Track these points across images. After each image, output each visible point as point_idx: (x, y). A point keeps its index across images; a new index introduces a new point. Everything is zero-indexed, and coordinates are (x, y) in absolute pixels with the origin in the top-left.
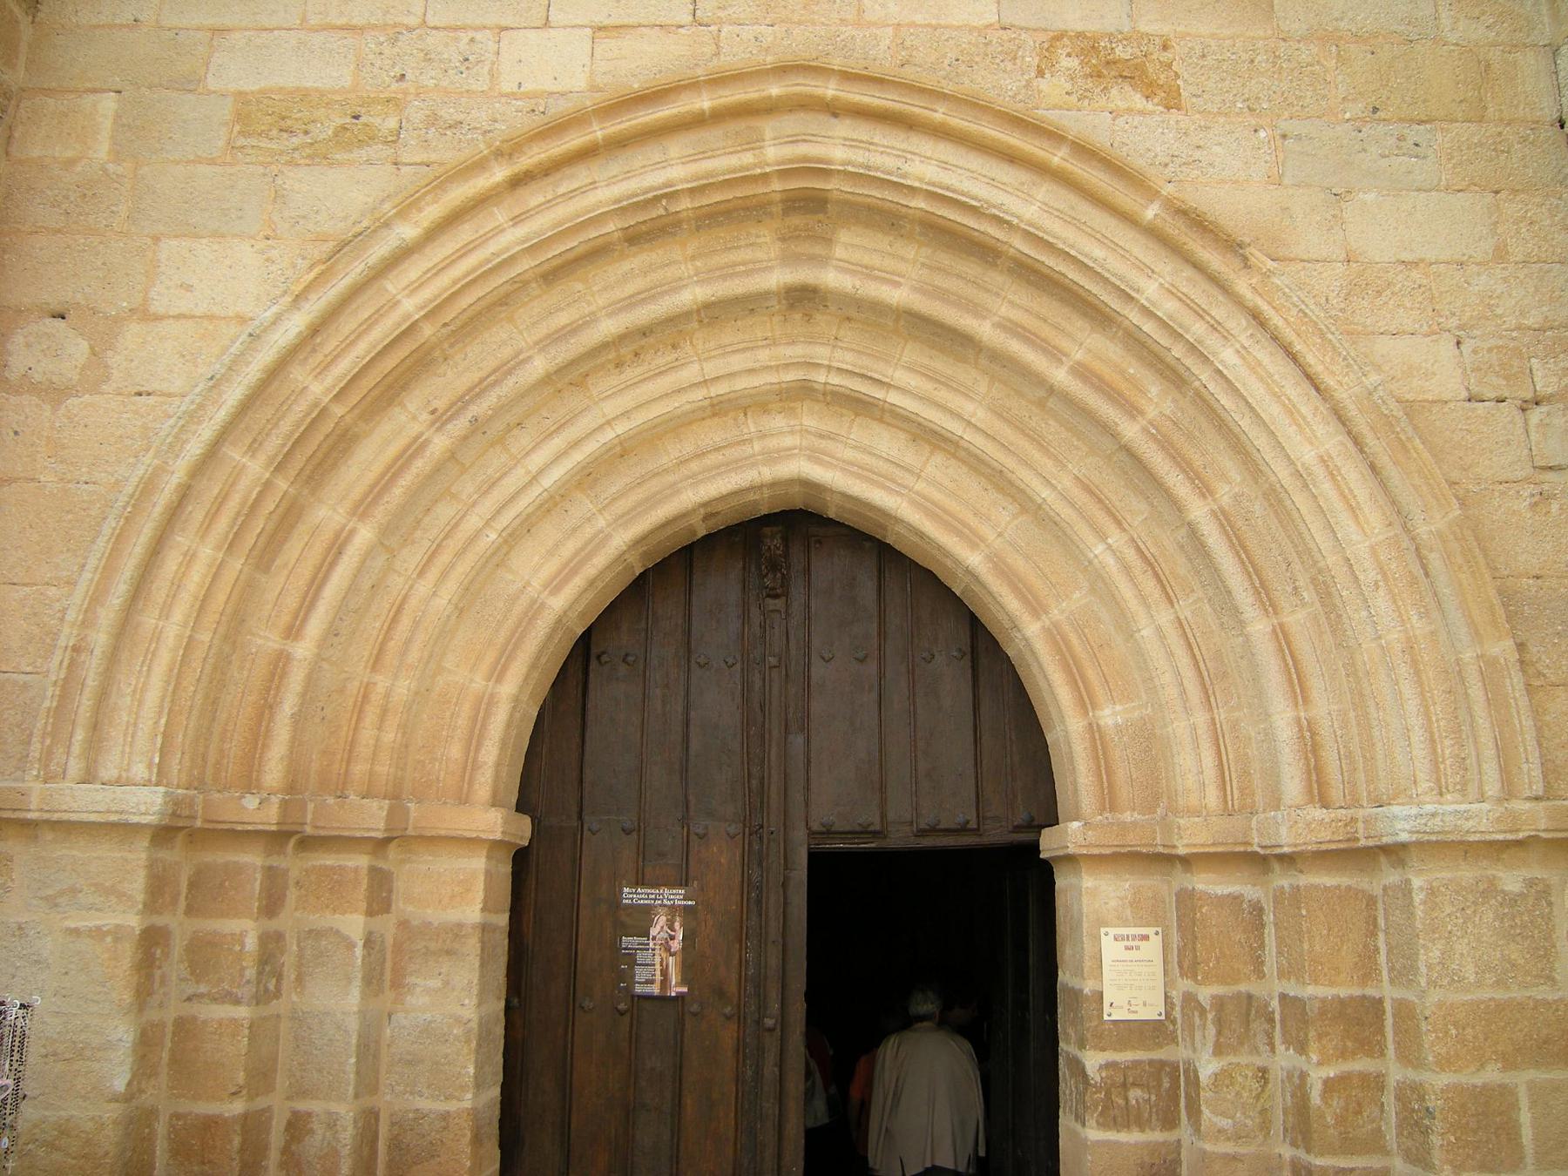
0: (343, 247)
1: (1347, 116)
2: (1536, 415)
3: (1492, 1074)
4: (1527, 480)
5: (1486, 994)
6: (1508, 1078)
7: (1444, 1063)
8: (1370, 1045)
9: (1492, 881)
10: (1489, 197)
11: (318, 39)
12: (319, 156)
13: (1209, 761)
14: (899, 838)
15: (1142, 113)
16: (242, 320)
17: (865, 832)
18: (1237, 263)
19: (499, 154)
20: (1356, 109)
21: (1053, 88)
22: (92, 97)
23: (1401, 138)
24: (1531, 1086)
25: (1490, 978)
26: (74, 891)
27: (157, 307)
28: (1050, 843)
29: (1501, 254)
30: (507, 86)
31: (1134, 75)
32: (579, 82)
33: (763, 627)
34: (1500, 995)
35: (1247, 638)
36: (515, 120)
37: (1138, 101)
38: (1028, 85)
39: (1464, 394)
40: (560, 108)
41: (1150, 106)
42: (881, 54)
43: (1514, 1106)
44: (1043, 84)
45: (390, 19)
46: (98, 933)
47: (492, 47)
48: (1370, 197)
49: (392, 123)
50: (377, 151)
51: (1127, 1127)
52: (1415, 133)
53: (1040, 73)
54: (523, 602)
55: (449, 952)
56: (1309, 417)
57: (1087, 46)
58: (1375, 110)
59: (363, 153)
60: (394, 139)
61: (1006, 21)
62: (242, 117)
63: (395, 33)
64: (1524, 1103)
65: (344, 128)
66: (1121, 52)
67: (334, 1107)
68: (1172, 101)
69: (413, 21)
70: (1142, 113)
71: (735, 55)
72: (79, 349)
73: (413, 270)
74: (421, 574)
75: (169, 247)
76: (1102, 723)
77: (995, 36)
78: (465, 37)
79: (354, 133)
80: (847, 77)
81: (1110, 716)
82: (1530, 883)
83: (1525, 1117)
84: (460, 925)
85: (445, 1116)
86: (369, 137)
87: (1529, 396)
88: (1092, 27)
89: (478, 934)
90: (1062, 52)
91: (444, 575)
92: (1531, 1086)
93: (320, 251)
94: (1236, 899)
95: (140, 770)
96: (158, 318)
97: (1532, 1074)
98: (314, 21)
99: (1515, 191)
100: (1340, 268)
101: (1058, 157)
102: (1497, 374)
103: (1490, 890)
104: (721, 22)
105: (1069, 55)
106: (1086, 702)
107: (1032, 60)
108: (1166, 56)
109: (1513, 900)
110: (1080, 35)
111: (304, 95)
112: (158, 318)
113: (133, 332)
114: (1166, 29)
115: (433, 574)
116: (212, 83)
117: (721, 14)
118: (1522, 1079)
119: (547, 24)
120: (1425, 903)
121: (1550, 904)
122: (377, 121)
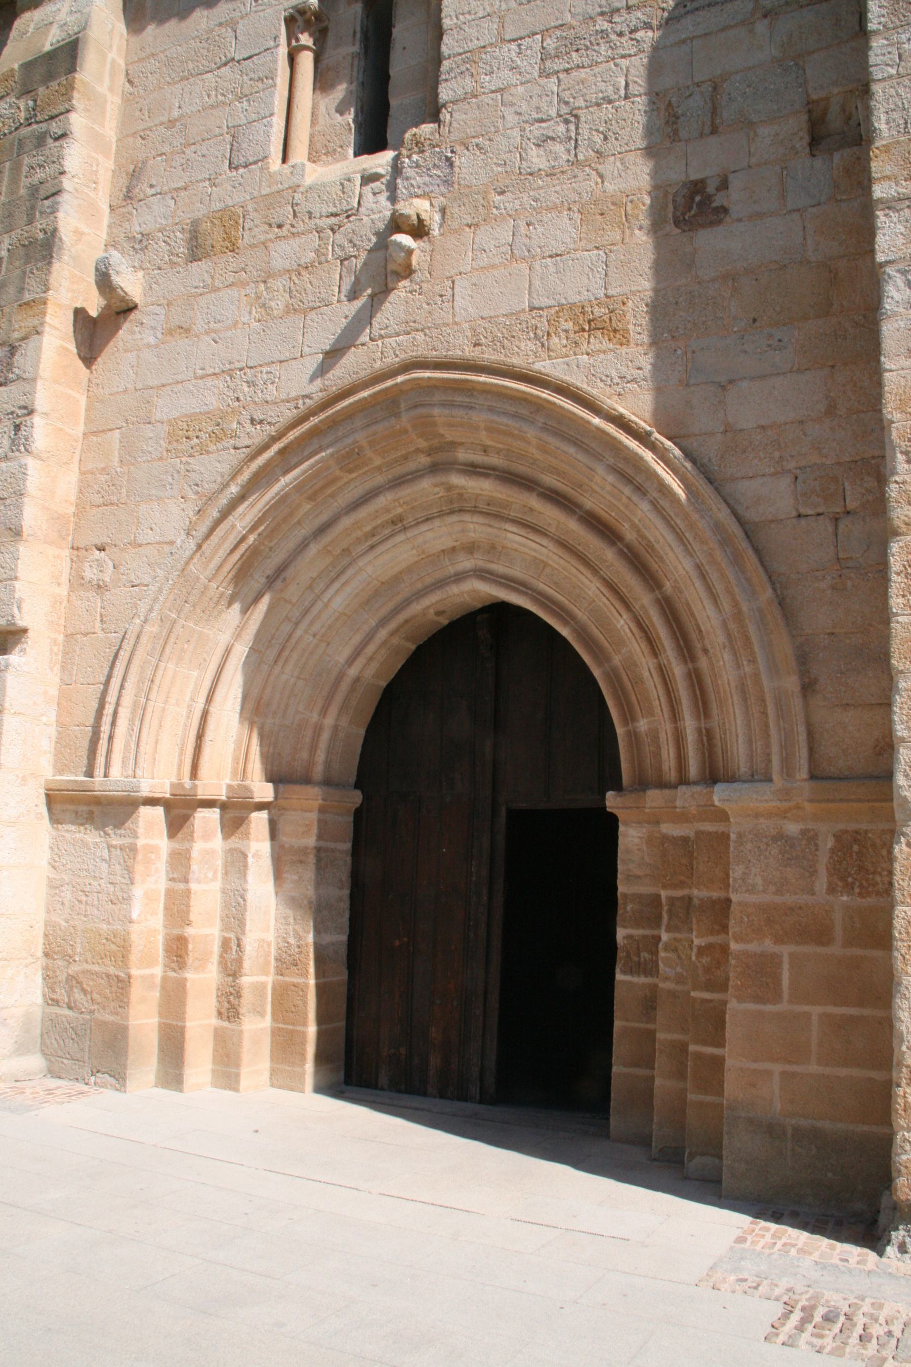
0: (211, 499)
1: (735, 329)
3: (769, 945)
5: (768, 898)
6: (777, 949)
7: (739, 939)
8: (656, 922)
25: (772, 888)
27: (140, 539)
29: (831, 410)
33: (287, 706)
34: (778, 899)
35: (337, 719)
36: (288, 414)
37: (606, 345)
39: (794, 514)
43: (779, 965)
51: (638, 974)
55: (301, 862)
56: (691, 540)
57: (577, 311)
58: (755, 320)
62: (172, 437)
64: (786, 966)
66: (599, 311)
74: (276, 662)
76: (638, 730)
80: (233, 477)
84: (306, 848)
89: (314, 851)
91: (286, 661)
92: (791, 955)
100: (719, 437)
102: (818, 496)
105: (566, 321)
110: (572, 305)
114: (626, 289)
115: (280, 663)
117: (383, 332)
118: (786, 950)
120: (736, 842)
121: (816, 845)
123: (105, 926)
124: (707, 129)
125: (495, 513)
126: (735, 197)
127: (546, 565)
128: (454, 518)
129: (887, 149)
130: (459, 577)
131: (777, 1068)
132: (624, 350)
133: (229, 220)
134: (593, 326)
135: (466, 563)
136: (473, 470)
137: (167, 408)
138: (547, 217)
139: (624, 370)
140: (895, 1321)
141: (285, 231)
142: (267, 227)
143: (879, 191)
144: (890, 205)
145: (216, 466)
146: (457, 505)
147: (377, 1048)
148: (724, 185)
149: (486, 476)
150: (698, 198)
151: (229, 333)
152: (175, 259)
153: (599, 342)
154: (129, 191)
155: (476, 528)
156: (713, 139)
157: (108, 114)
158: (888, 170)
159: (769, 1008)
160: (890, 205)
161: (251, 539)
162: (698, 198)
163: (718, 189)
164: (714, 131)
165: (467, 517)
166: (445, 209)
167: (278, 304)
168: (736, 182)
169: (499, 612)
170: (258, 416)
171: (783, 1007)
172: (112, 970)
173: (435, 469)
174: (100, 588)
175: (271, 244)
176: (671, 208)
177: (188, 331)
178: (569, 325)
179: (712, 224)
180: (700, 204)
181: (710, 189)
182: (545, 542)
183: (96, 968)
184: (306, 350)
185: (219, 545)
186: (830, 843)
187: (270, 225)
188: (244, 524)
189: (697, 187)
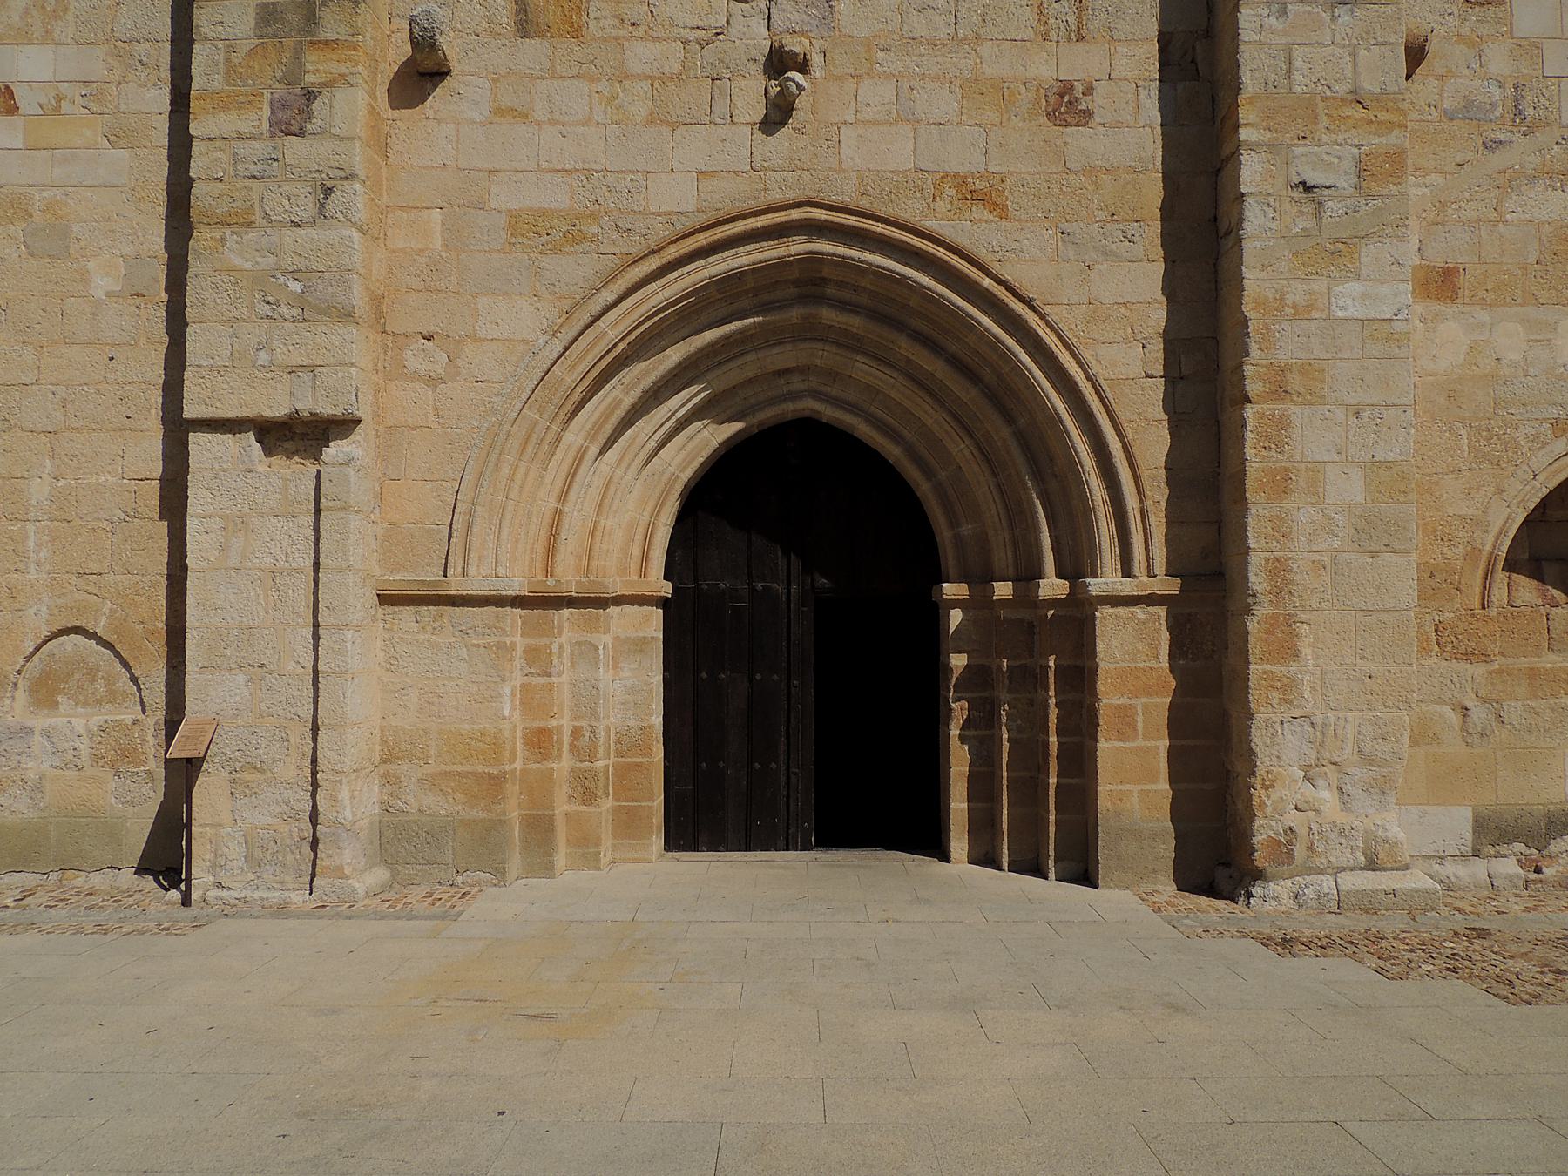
6: (1133, 701)
12: (557, 250)
13: (1010, 553)
24: (1145, 706)
27: (481, 334)
30: (654, 209)
32: (690, 206)
36: (662, 232)
37: (986, 215)
42: (846, 194)
45: (587, 166)
54: (667, 475)
57: (961, 181)
60: (595, 239)
62: (512, 227)
66: (979, 185)
67: (562, 722)
69: (599, 167)
71: (775, 196)
73: (612, 315)
79: (574, 237)
81: (967, 529)
83: (1140, 719)
92: (1145, 706)
94: (1021, 621)
96: (483, 341)
97: (1144, 700)
98: (545, 165)
106: (953, 523)
110: (956, 174)
111: (543, 213)
114: (1004, 169)
123: (466, 726)
125: (850, 343)
126: (1098, 103)
127: (878, 392)
128: (807, 345)
129: (1251, 100)
130: (793, 396)
131: (1135, 788)
134: (978, 198)
135: (798, 384)
136: (842, 305)
137: (503, 198)
138: (930, 85)
139: (1003, 240)
140: (175, 895)
141: (641, 30)
142: (617, 22)
143: (1244, 134)
144: (1251, 147)
145: (575, 270)
146: (810, 333)
147: (711, 802)
148: (1089, 91)
149: (857, 313)
151: (580, 129)
152: (498, 29)
153: (980, 212)
155: (824, 355)
158: (1252, 118)
159: (1128, 745)
160: (1251, 147)
161: (621, 346)
165: (820, 346)
167: (640, 111)
168: (1101, 89)
169: (808, 426)
170: (624, 224)
171: (1140, 742)
172: (480, 769)
173: (804, 299)
174: (432, 381)
175: (626, 44)
177: (524, 115)
178: (953, 192)
182: (895, 375)
183: (459, 768)
184: (677, 166)
185: (587, 351)
188: (616, 332)
189: (1066, 88)
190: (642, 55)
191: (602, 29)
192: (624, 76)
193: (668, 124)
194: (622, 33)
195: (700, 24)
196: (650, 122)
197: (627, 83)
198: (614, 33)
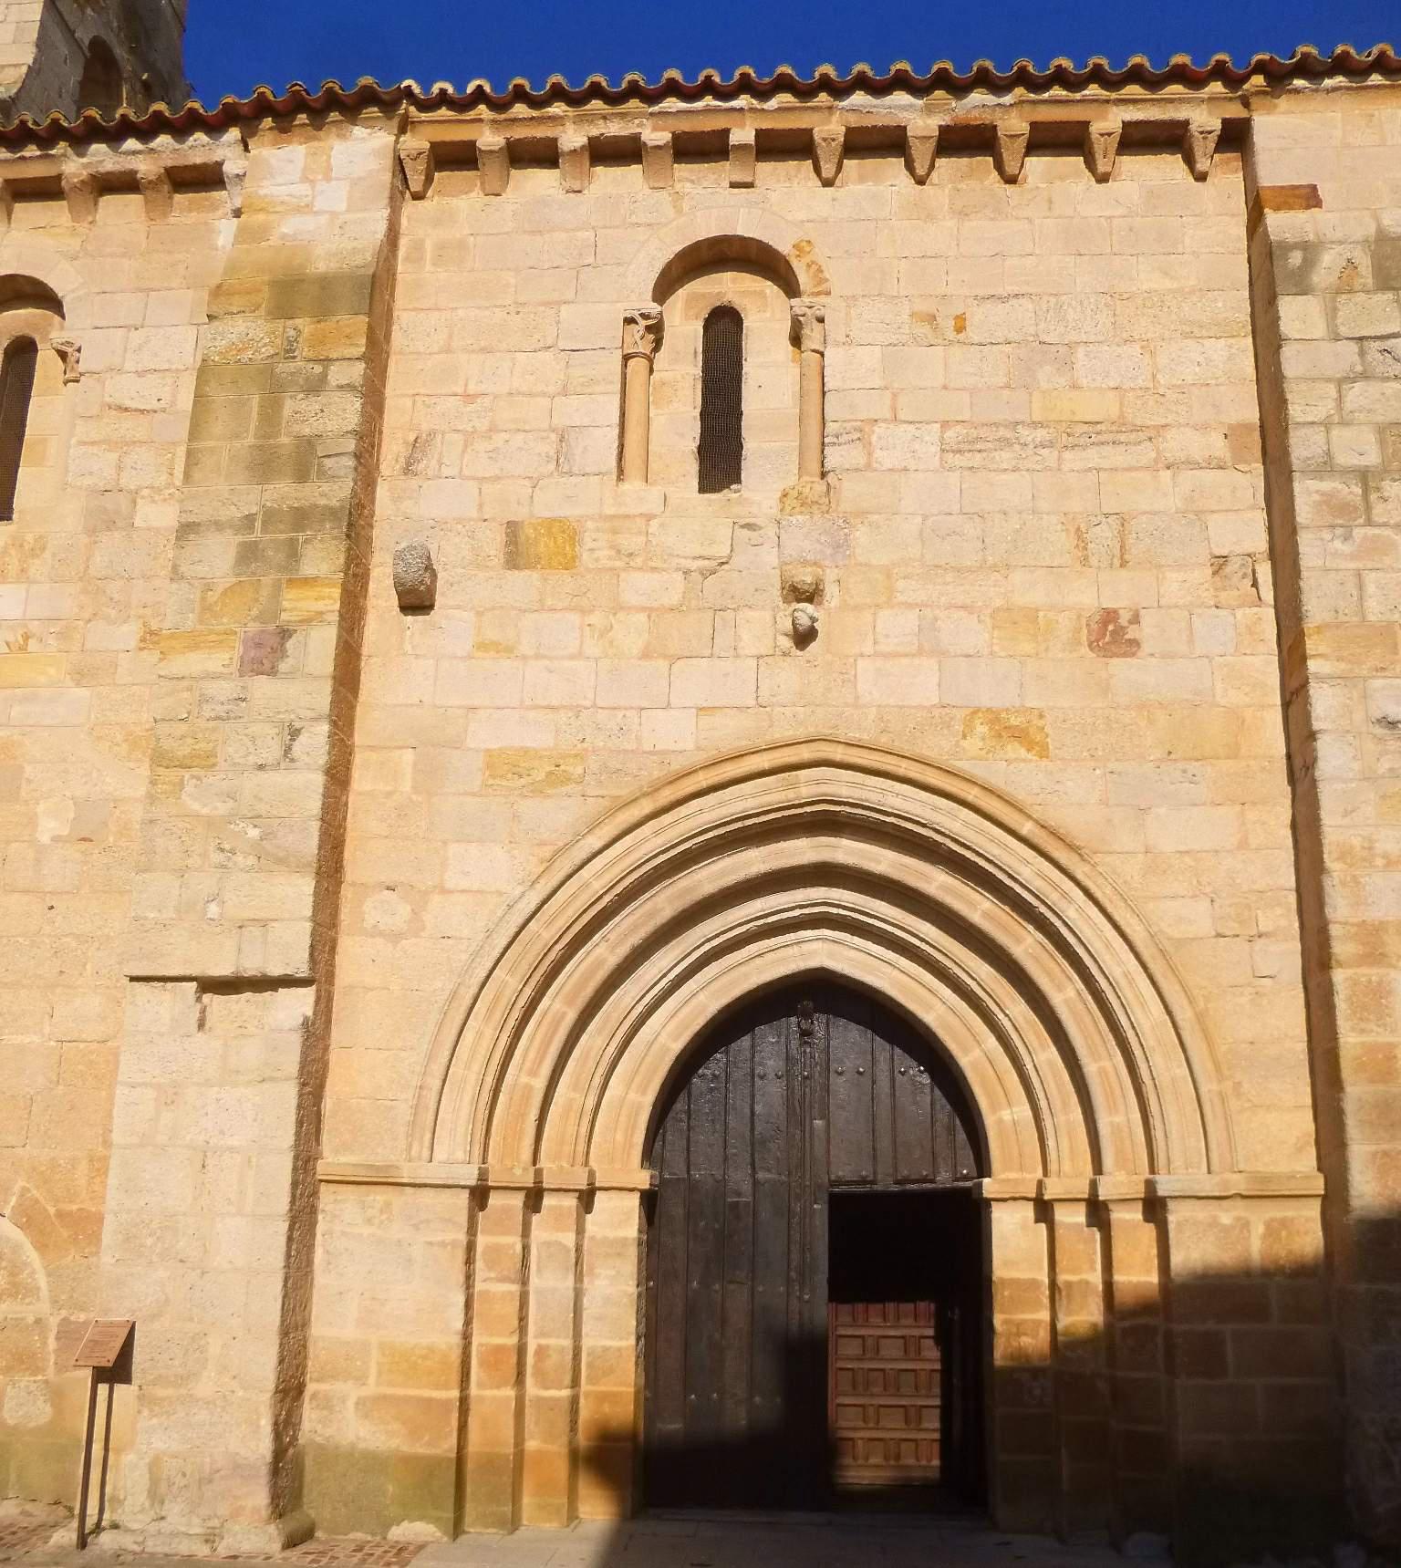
2: (1259, 943)
3: (1211, 1325)
4: (1249, 985)
9: (1215, 1218)
10: (1238, 808)
11: (532, 715)
12: (537, 791)
14: (885, 1184)
15: (1024, 761)
16: (500, 894)
17: (864, 1181)
18: (1077, 858)
19: (646, 795)
20: (1158, 753)
21: (973, 744)
22: (398, 752)
23: (1184, 771)
26: (428, 1221)
27: (449, 885)
28: (989, 1187)
30: (647, 747)
31: (1020, 736)
37: (1023, 752)
38: (957, 744)
40: (677, 765)
41: (1029, 756)
44: (964, 743)
46: (443, 1244)
47: (636, 720)
48: (1162, 811)
49: (580, 770)
50: (570, 788)
52: (1193, 767)
53: (964, 737)
59: (564, 789)
61: (945, 702)
63: (577, 711)
65: (551, 773)
66: (1014, 721)
68: (1044, 753)
69: (588, 703)
70: (1024, 761)
72: (404, 910)
75: (453, 849)
77: (936, 712)
78: (620, 714)
79: (557, 778)
82: (1238, 1219)
85: (619, 1349)
86: (567, 779)
87: (1254, 932)
88: (996, 704)
90: (978, 722)
93: (547, 852)
95: (460, 1155)
96: (451, 892)
99: (1254, 803)
100: (1141, 856)
101: (972, 794)
103: (1214, 1223)
104: (772, 705)
107: (959, 727)
108: (1040, 723)
109: (1226, 1230)
112: (451, 892)
113: (436, 899)
116: (470, 743)
119: (668, 706)
122: (570, 769)
124: (1117, 562)
129: (1319, 629)
132: (1045, 762)
133: (567, 533)
141: (639, 561)
142: (613, 553)
148: (1135, 619)
150: (1111, 627)
151: (567, 664)
153: (1015, 750)
154: (409, 464)
156: (1123, 572)
157: (1365, 970)
158: (1322, 649)
162: (1111, 627)
163: (1130, 622)
164: (1123, 564)
166: (794, 589)
168: (1147, 619)
176: (1085, 631)
179: (1125, 655)
180: (1113, 632)
181: (1123, 621)
186: (1261, 1229)
187: (619, 552)
189: (1109, 616)
190: (639, 586)
191: (597, 560)
192: (618, 608)
193: (665, 657)
194: (618, 564)
195: (705, 553)
196: (646, 655)
197: (621, 615)
198: (610, 564)
